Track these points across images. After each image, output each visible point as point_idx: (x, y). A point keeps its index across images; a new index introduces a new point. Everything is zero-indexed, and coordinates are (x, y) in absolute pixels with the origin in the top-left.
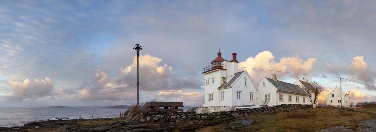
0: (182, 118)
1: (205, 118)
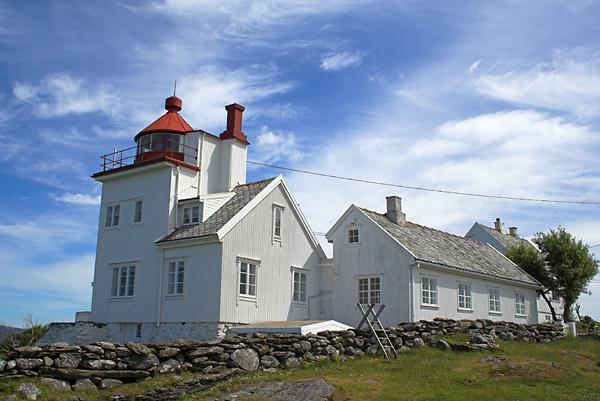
1: (103, 367)
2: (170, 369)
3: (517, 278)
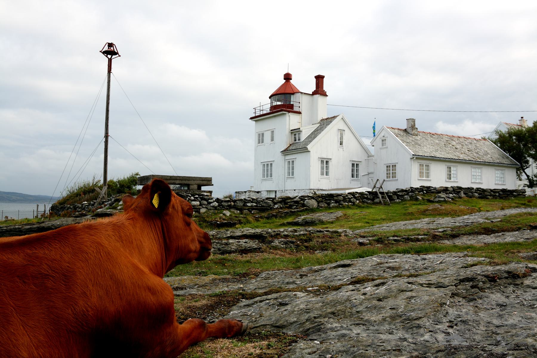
0: (211, 205)
1: (252, 206)
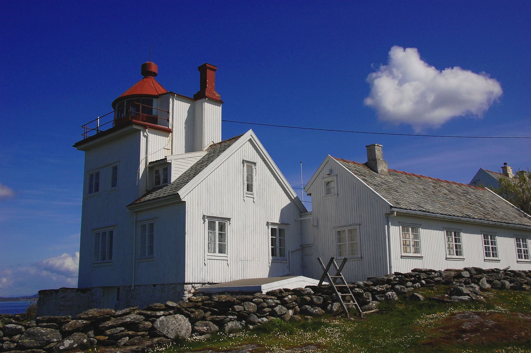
2: (71, 345)
3: (517, 221)
